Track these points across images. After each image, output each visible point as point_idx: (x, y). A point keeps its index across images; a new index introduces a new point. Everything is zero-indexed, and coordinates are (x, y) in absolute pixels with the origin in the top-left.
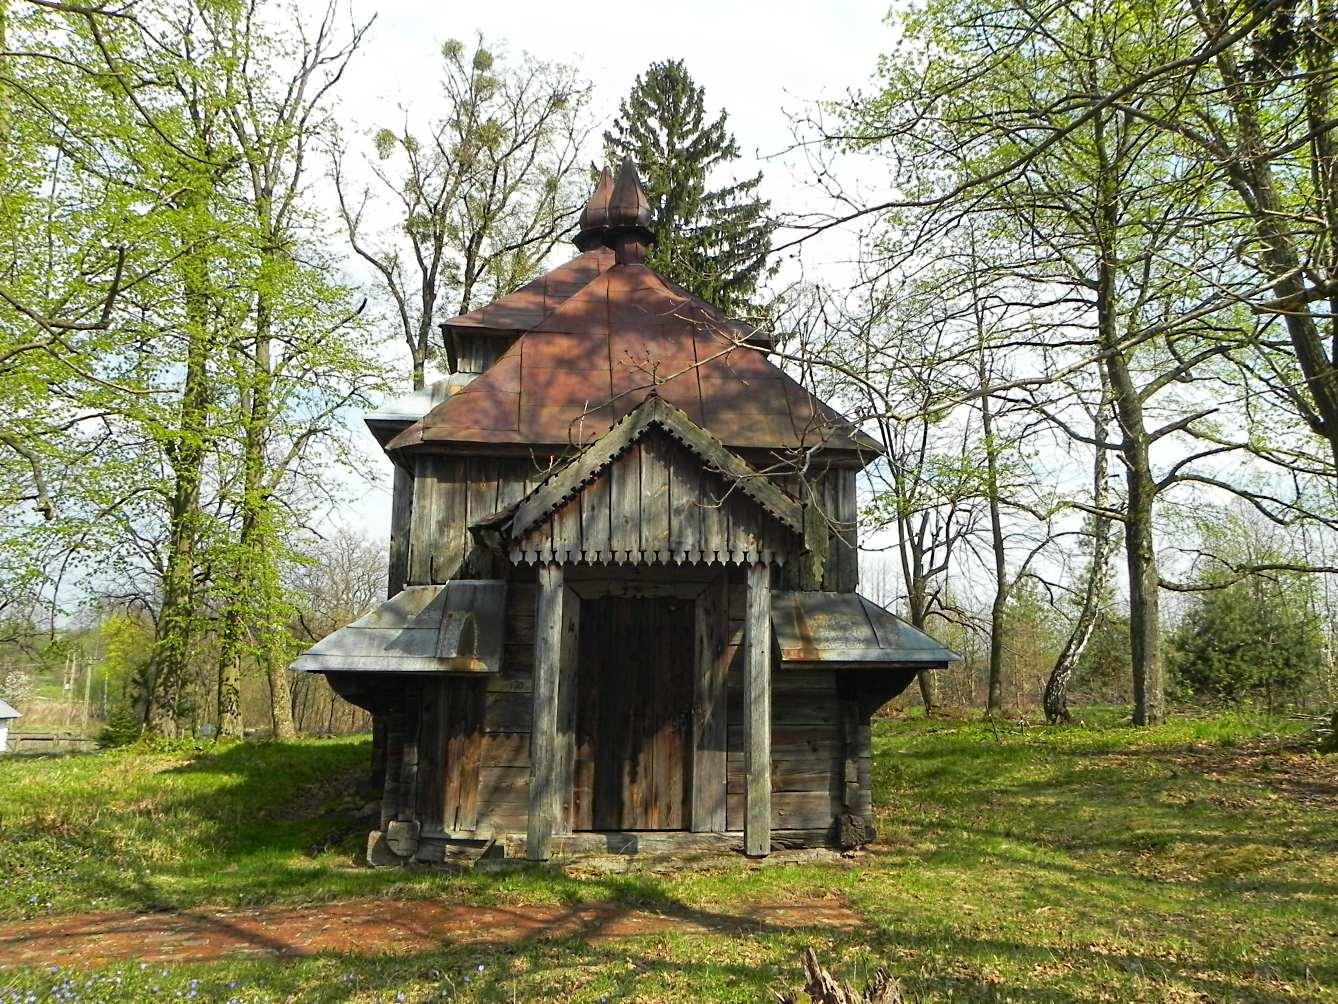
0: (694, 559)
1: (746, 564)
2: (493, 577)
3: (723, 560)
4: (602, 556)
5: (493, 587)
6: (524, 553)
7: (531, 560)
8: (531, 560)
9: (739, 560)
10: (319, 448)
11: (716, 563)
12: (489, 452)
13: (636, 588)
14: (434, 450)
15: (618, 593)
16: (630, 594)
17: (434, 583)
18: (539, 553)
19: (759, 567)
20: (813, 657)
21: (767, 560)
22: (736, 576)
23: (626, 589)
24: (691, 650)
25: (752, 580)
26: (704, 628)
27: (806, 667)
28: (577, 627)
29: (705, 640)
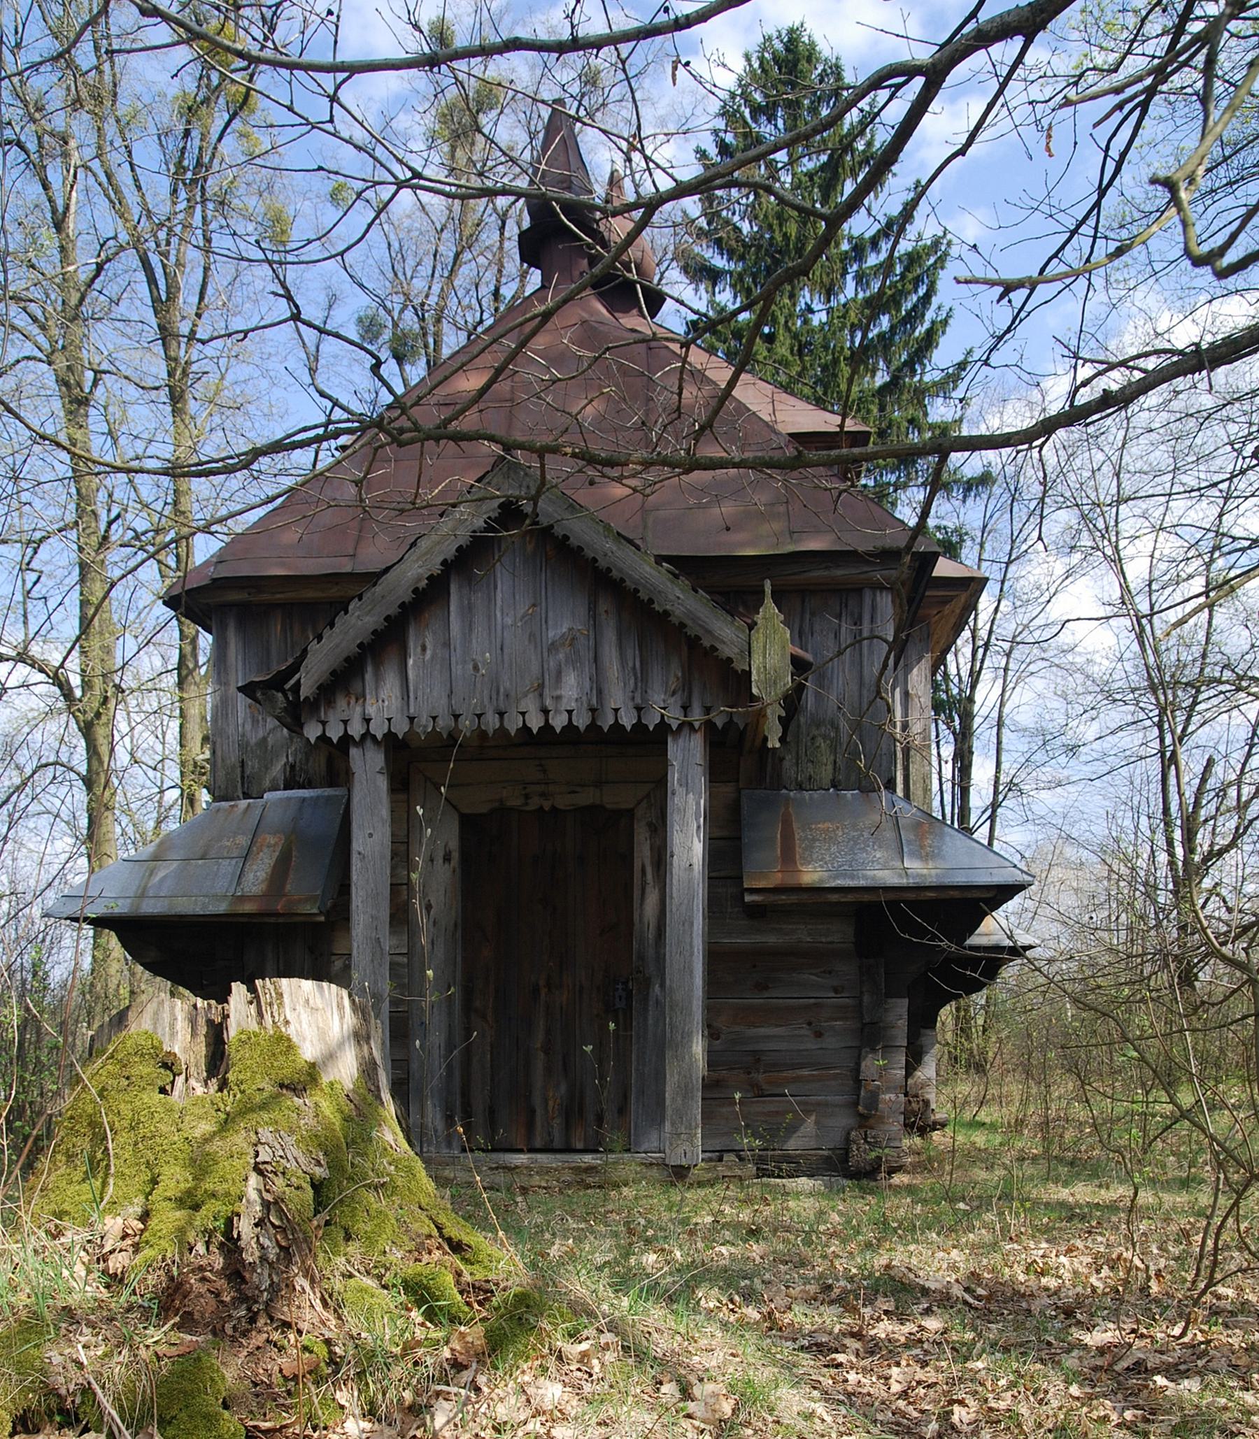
0: (581, 722)
1: (663, 726)
2: (331, 785)
3: (628, 721)
4: (440, 722)
5: (329, 798)
6: (324, 723)
7: (335, 734)
8: (335, 734)
9: (652, 721)
10: (1070, 1086)
11: (617, 726)
12: (310, 594)
13: (543, 795)
14: (234, 596)
15: (516, 802)
16: (534, 803)
17: (247, 796)
18: (345, 722)
19: (686, 730)
20: (791, 881)
21: (697, 716)
22: (648, 743)
23: (527, 797)
24: (628, 887)
25: (675, 750)
26: (648, 853)
27: (793, 898)
28: (456, 855)
29: (649, 870)
